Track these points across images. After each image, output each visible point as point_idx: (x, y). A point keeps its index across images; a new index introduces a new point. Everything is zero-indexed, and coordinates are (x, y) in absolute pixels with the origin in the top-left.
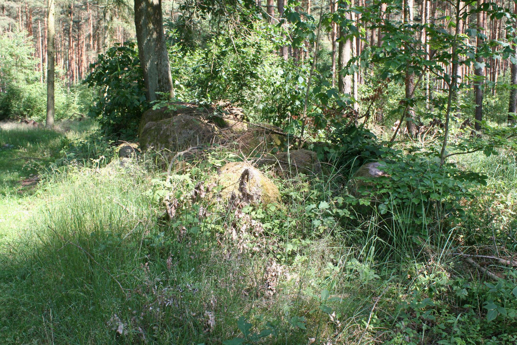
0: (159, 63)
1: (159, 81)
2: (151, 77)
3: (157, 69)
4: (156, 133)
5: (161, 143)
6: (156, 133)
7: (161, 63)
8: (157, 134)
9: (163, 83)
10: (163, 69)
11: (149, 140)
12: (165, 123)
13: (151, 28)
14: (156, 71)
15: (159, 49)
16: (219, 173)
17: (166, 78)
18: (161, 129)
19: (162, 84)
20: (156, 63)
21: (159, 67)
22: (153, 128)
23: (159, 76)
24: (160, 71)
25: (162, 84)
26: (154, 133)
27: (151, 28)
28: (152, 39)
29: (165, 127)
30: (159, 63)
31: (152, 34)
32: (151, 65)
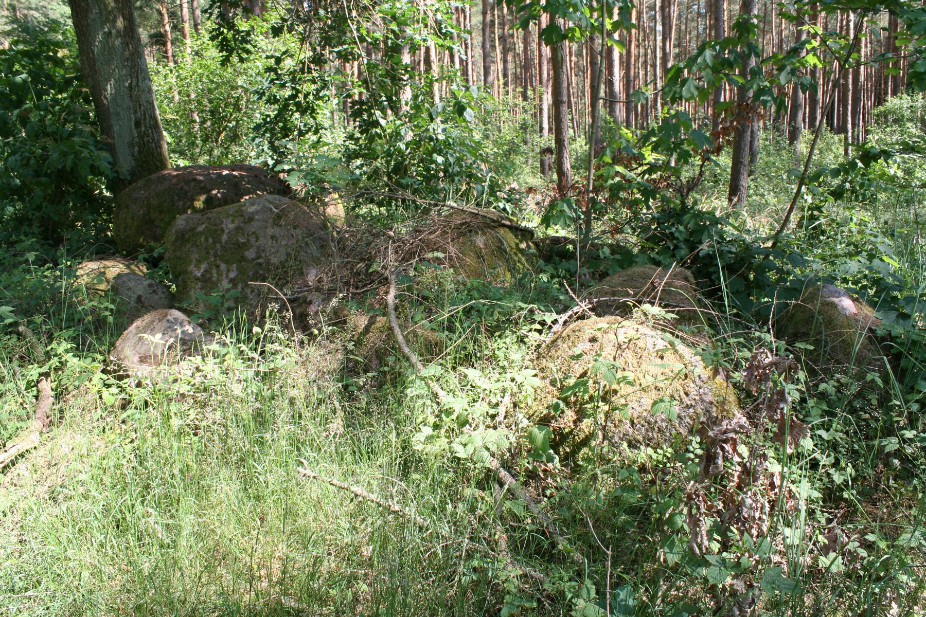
0: (134, 84)
1: (138, 124)
2: (118, 114)
3: (131, 97)
4: (210, 240)
5: (227, 262)
6: (210, 240)
7: (138, 86)
8: (214, 243)
9: (146, 127)
10: (143, 96)
11: (195, 256)
12: (228, 216)
13: (110, 8)
14: (128, 102)
15: (132, 54)
16: (810, 496)
17: (151, 117)
18: (223, 231)
19: (143, 129)
20: (127, 84)
21: (134, 93)
22: (200, 229)
23: (135, 112)
24: (137, 102)
25: (143, 129)
26: (206, 240)
27: (110, 8)
28: (114, 31)
29: (231, 226)
30: (134, 84)
31: (114, 21)
32: (117, 89)
